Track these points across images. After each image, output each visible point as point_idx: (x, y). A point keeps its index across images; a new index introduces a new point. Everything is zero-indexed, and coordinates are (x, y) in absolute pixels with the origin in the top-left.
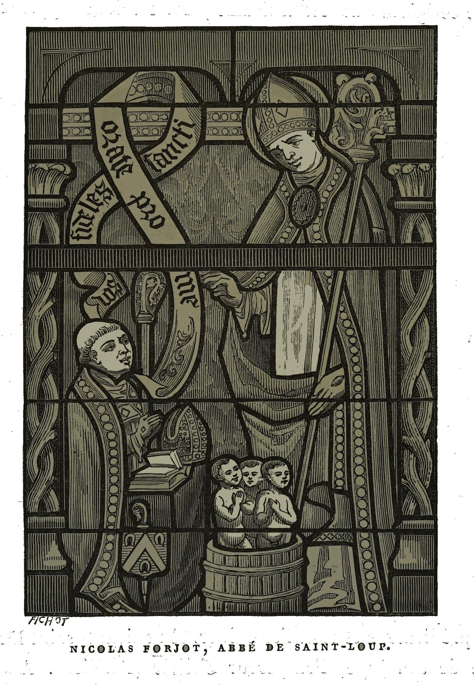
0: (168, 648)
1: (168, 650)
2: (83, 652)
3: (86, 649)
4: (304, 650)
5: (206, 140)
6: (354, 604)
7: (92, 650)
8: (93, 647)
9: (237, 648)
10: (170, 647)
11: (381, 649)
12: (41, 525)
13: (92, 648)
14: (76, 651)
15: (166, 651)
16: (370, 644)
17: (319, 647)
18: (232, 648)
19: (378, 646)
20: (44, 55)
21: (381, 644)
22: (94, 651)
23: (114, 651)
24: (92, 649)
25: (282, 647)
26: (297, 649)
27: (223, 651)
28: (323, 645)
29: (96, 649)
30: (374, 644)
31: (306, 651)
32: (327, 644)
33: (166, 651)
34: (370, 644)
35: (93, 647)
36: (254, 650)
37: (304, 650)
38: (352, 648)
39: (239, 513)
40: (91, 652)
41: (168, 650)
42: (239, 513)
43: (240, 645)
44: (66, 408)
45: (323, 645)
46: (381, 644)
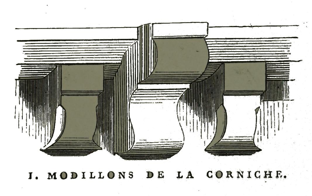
1: (229, 176)
2: (249, 177)
3: (252, 175)
4: (188, 177)
5: (225, 97)
7: (210, 176)
8: (211, 172)
9: (235, 174)
10: (231, 173)
13: (210, 173)
14: (124, 177)
15: (228, 177)
17: (246, 175)
20: (114, 77)
22: (212, 177)
23: (94, 178)
24: (258, 175)
25: (281, 174)
26: (131, 176)
28: (120, 173)
29: (214, 174)
32: (124, 173)
33: (228, 177)
35: (211, 172)
36: (163, 177)
37: (188, 177)
38: (180, 176)
40: (209, 177)
41: (229, 176)
42: (63, 110)
44: (63, 91)
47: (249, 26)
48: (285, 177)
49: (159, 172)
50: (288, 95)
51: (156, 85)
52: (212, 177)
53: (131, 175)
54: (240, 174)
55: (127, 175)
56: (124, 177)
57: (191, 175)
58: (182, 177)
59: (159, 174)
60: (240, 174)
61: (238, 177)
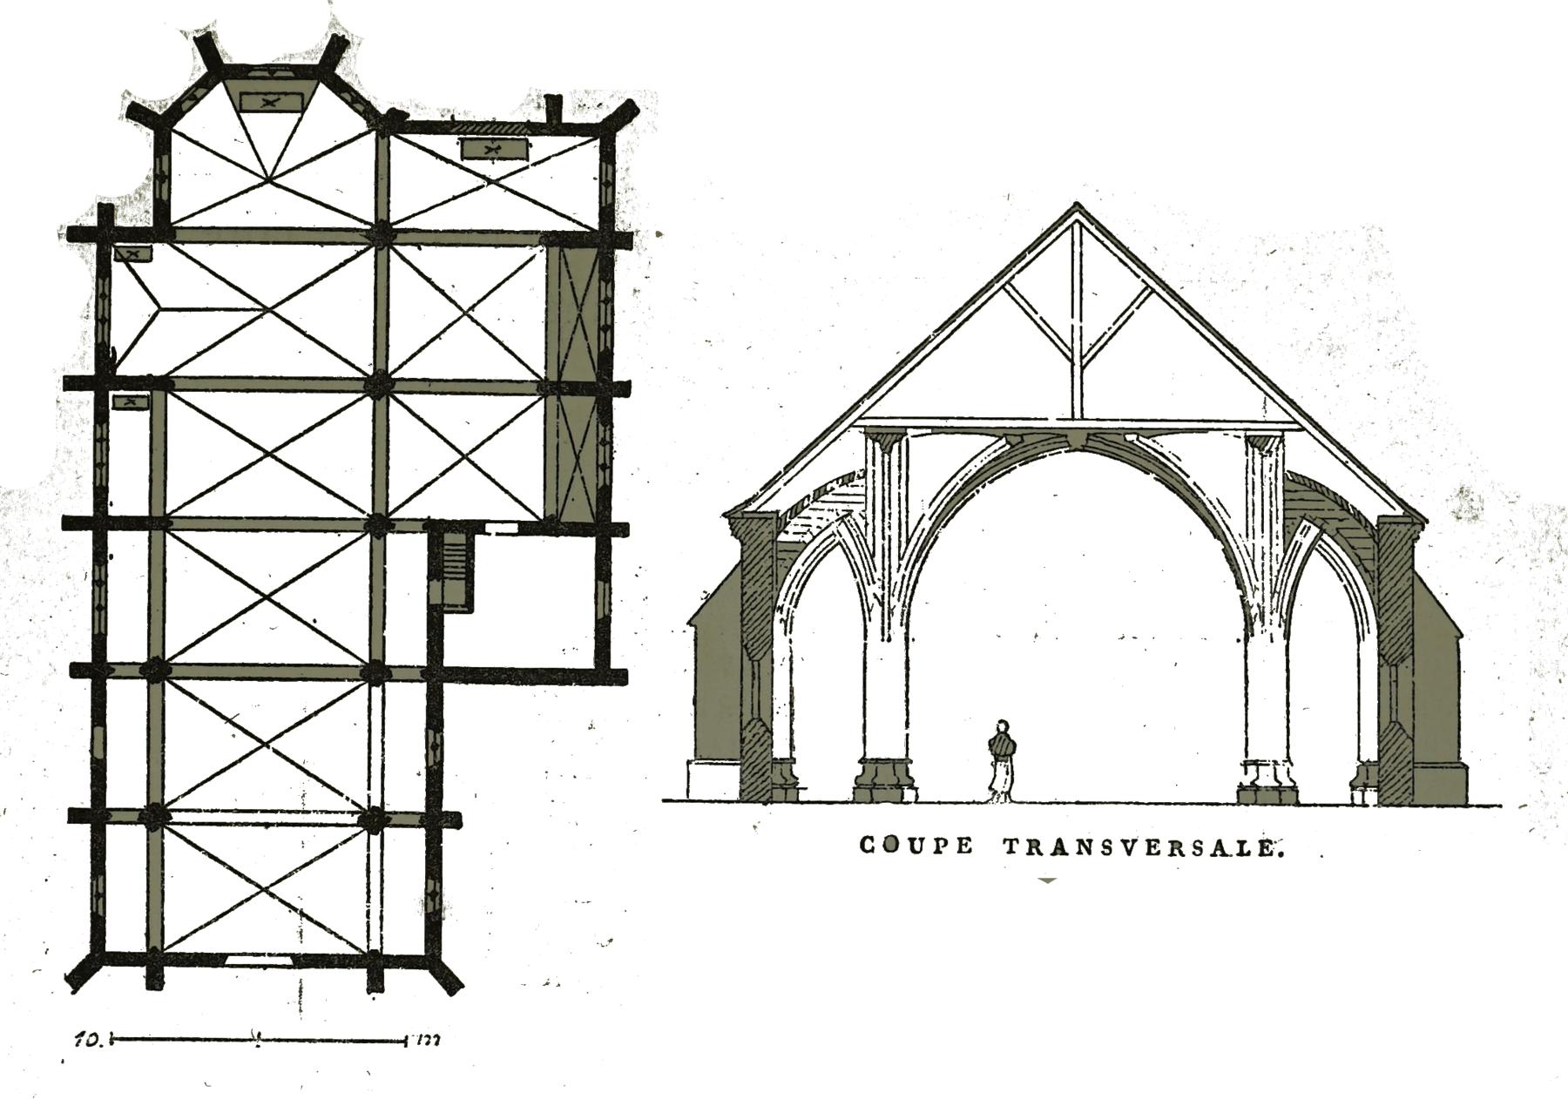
0: (1176, 846)
4: (1214, 855)
6: (242, 94)
8: (872, 838)
10: (1038, 843)
11: (938, 851)
12: (445, 987)
13: (868, 842)
14: (1089, 852)
16: (912, 840)
18: (1107, 848)
19: (930, 845)
21: (937, 840)
22: (872, 850)
25: (970, 845)
27: (1064, 853)
28: (1081, 842)
30: (922, 840)
31: (1219, 858)
34: (912, 840)
37: (1214, 855)
39: (232, 966)
42: (232, 966)
43: (1172, 842)
45: (1081, 842)
46: (937, 840)
47: (310, 919)
48: (1281, 854)
49: (960, 839)
50: (1190, 482)
51: (233, 246)
52: (872, 850)
53: (963, 843)
54: (1085, 846)
55: (1097, 847)
56: (1089, 852)
57: (1062, 848)
58: (1249, 854)
59: (1150, 847)
60: (1085, 846)
61: (1080, 853)
